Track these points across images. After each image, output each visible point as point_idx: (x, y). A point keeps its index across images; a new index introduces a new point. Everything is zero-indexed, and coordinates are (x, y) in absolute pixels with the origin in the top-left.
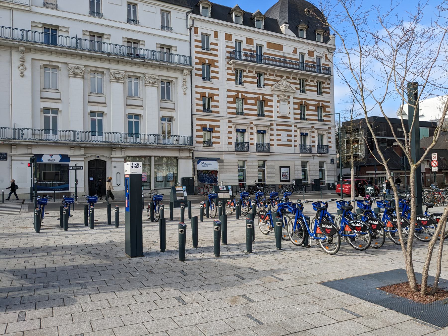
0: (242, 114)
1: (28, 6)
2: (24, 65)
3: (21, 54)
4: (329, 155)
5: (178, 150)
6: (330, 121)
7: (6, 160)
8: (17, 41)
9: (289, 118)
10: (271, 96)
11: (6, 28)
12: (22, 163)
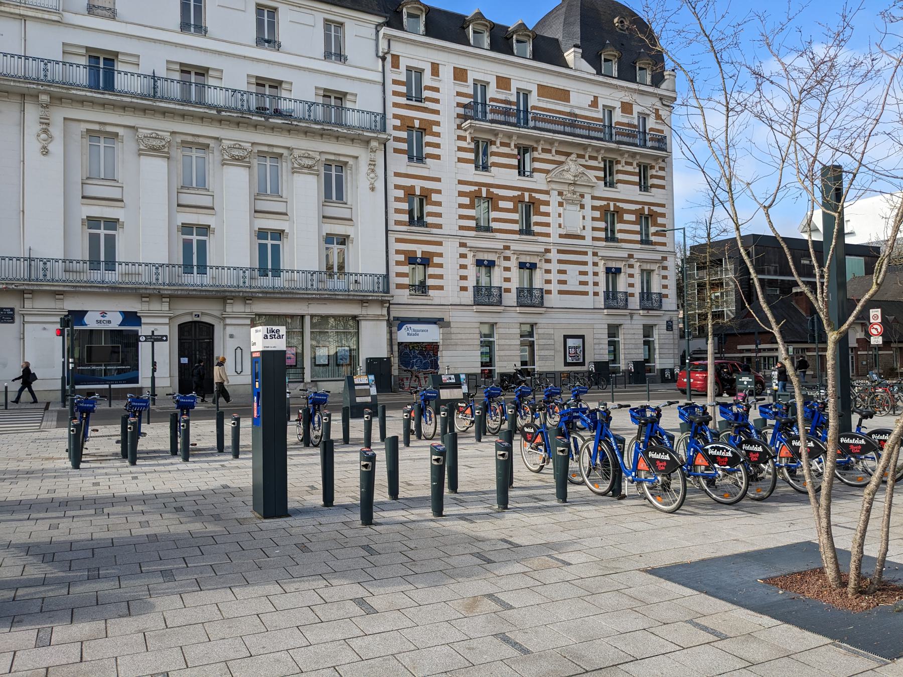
0: (488, 229)
1: (57, 11)
2: (48, 130)
3: (42, 109)
4: (663, 312)
5: (359, 303)
6: (664, 244)
7: (13, 322)
8: (33, 84)
9: (583, 238)
10: (547, 192)
11: (12, 56)
12: (45, 329)
